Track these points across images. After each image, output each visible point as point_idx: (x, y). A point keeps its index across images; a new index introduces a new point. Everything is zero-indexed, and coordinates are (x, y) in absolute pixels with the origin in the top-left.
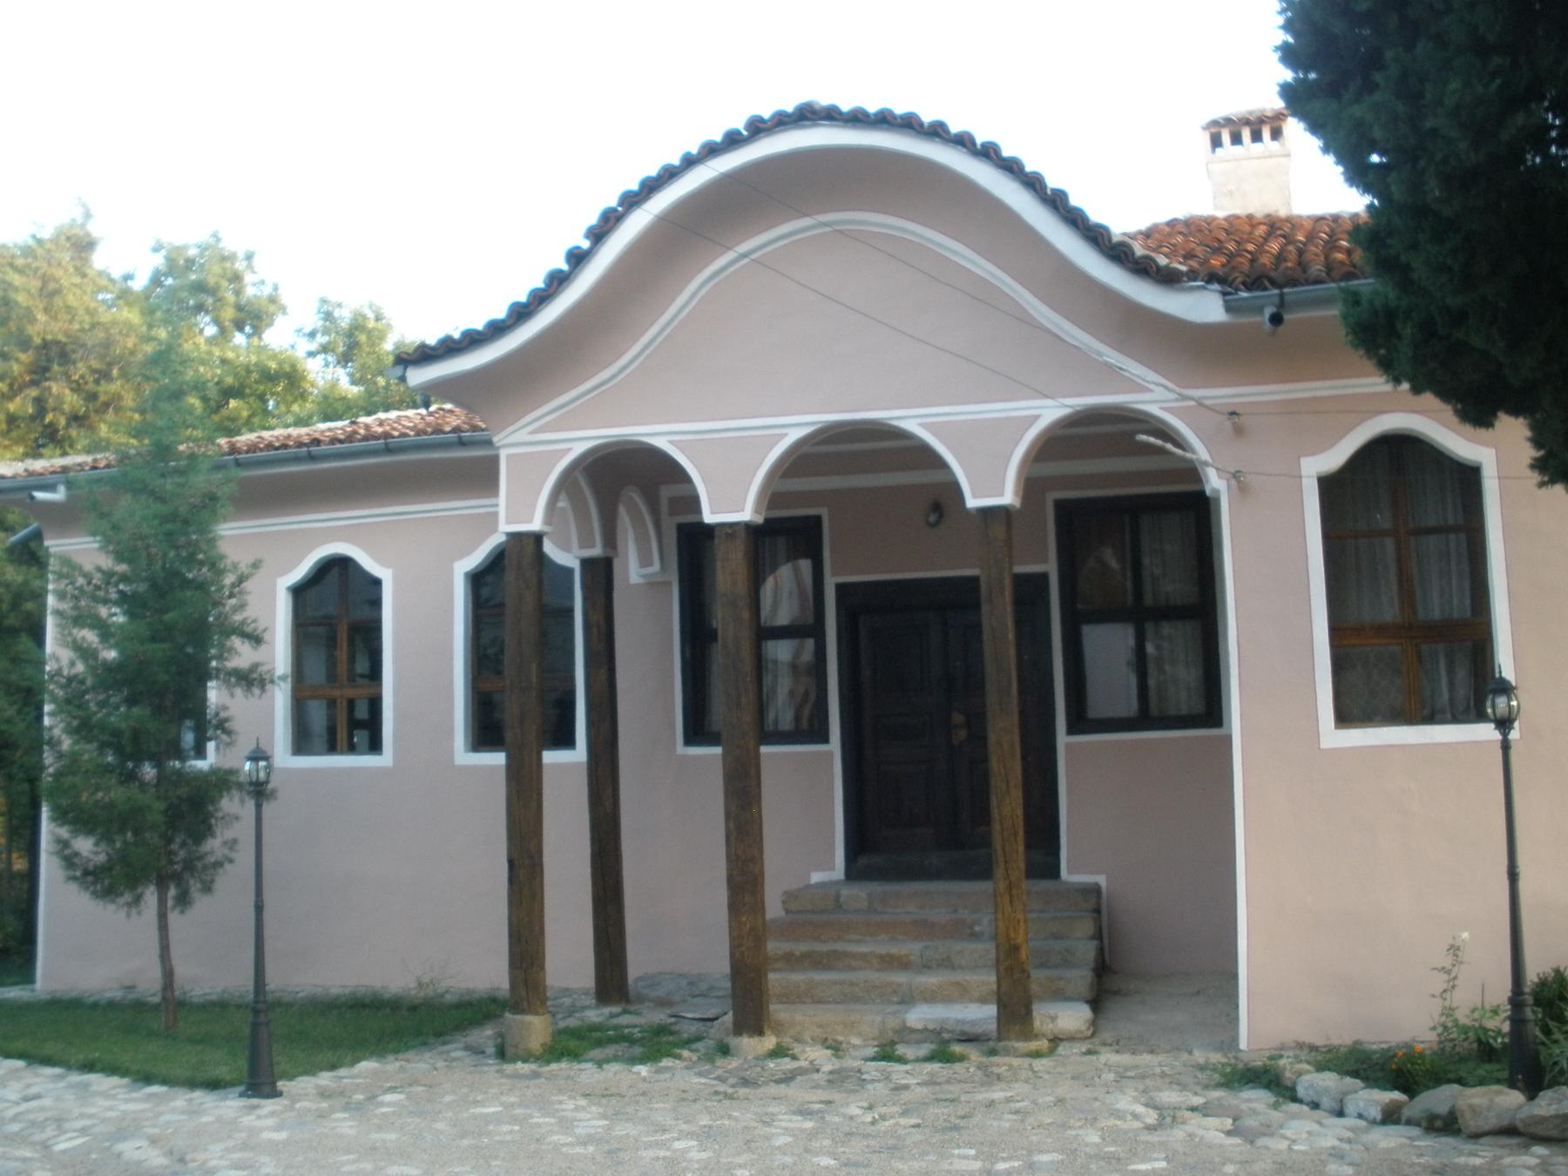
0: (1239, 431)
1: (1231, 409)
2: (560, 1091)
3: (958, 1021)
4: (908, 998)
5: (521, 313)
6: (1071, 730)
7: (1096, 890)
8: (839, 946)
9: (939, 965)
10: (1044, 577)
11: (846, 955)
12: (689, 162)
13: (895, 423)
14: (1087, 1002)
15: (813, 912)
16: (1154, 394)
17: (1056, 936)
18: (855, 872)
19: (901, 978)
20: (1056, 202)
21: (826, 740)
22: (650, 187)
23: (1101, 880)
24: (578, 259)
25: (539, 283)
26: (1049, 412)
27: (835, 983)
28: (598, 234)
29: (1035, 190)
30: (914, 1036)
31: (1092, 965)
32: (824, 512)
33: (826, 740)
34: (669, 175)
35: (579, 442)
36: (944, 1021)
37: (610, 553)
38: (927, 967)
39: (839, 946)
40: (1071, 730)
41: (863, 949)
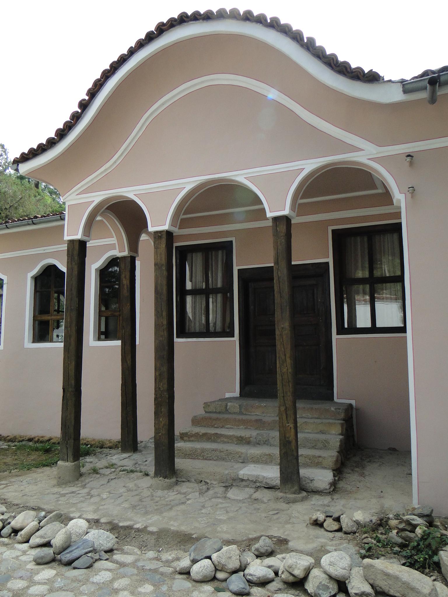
0: (411, 164)
1: (408, 154)
2: (251, 426)
3: (264, 477)
4: (245, 461)
5: (61, 134)
6: (338, 333)
7: (351, 405)
8: (219, 431)
9: (264, 443)
10: (327, 263)
11: (222, 435)
12: (132, 52)
13: (233, 178)
14: (333, 470)
15: (216, 412)
16: (365, 153)
17: (322, 432)
18: (243, 394)
19: (243, 449)
20: (310, 47)
21: (233, 336)
22: (115, 67)
23: (353, 402)
24: (84, 105)
25: (67, 118)
26: (309, 166)
27: (214, 450)
28: (93, 93)
29: (298, 41)
30: (244, 483)
31: (338, 449)
32: (233, 239)
33: (233, 336)
34: (123, 60)
35: (97, 198)
36: (258, 477)
37: (133, 254)
38: (258, 444)
39: (219, 431)
40: (338, 333)
41: (231, 433)
